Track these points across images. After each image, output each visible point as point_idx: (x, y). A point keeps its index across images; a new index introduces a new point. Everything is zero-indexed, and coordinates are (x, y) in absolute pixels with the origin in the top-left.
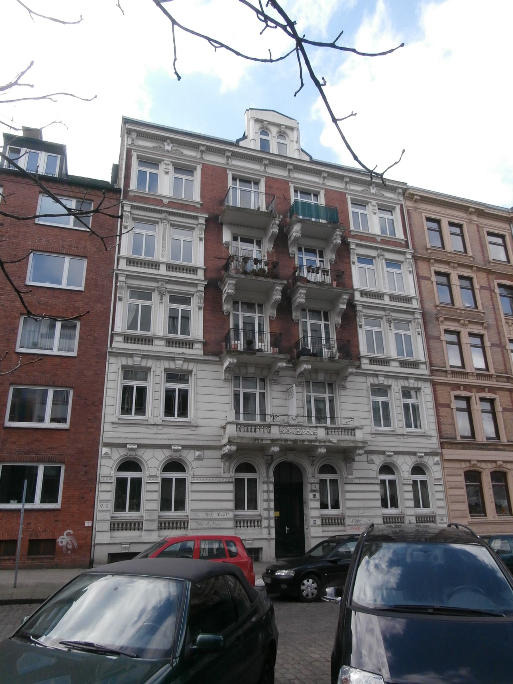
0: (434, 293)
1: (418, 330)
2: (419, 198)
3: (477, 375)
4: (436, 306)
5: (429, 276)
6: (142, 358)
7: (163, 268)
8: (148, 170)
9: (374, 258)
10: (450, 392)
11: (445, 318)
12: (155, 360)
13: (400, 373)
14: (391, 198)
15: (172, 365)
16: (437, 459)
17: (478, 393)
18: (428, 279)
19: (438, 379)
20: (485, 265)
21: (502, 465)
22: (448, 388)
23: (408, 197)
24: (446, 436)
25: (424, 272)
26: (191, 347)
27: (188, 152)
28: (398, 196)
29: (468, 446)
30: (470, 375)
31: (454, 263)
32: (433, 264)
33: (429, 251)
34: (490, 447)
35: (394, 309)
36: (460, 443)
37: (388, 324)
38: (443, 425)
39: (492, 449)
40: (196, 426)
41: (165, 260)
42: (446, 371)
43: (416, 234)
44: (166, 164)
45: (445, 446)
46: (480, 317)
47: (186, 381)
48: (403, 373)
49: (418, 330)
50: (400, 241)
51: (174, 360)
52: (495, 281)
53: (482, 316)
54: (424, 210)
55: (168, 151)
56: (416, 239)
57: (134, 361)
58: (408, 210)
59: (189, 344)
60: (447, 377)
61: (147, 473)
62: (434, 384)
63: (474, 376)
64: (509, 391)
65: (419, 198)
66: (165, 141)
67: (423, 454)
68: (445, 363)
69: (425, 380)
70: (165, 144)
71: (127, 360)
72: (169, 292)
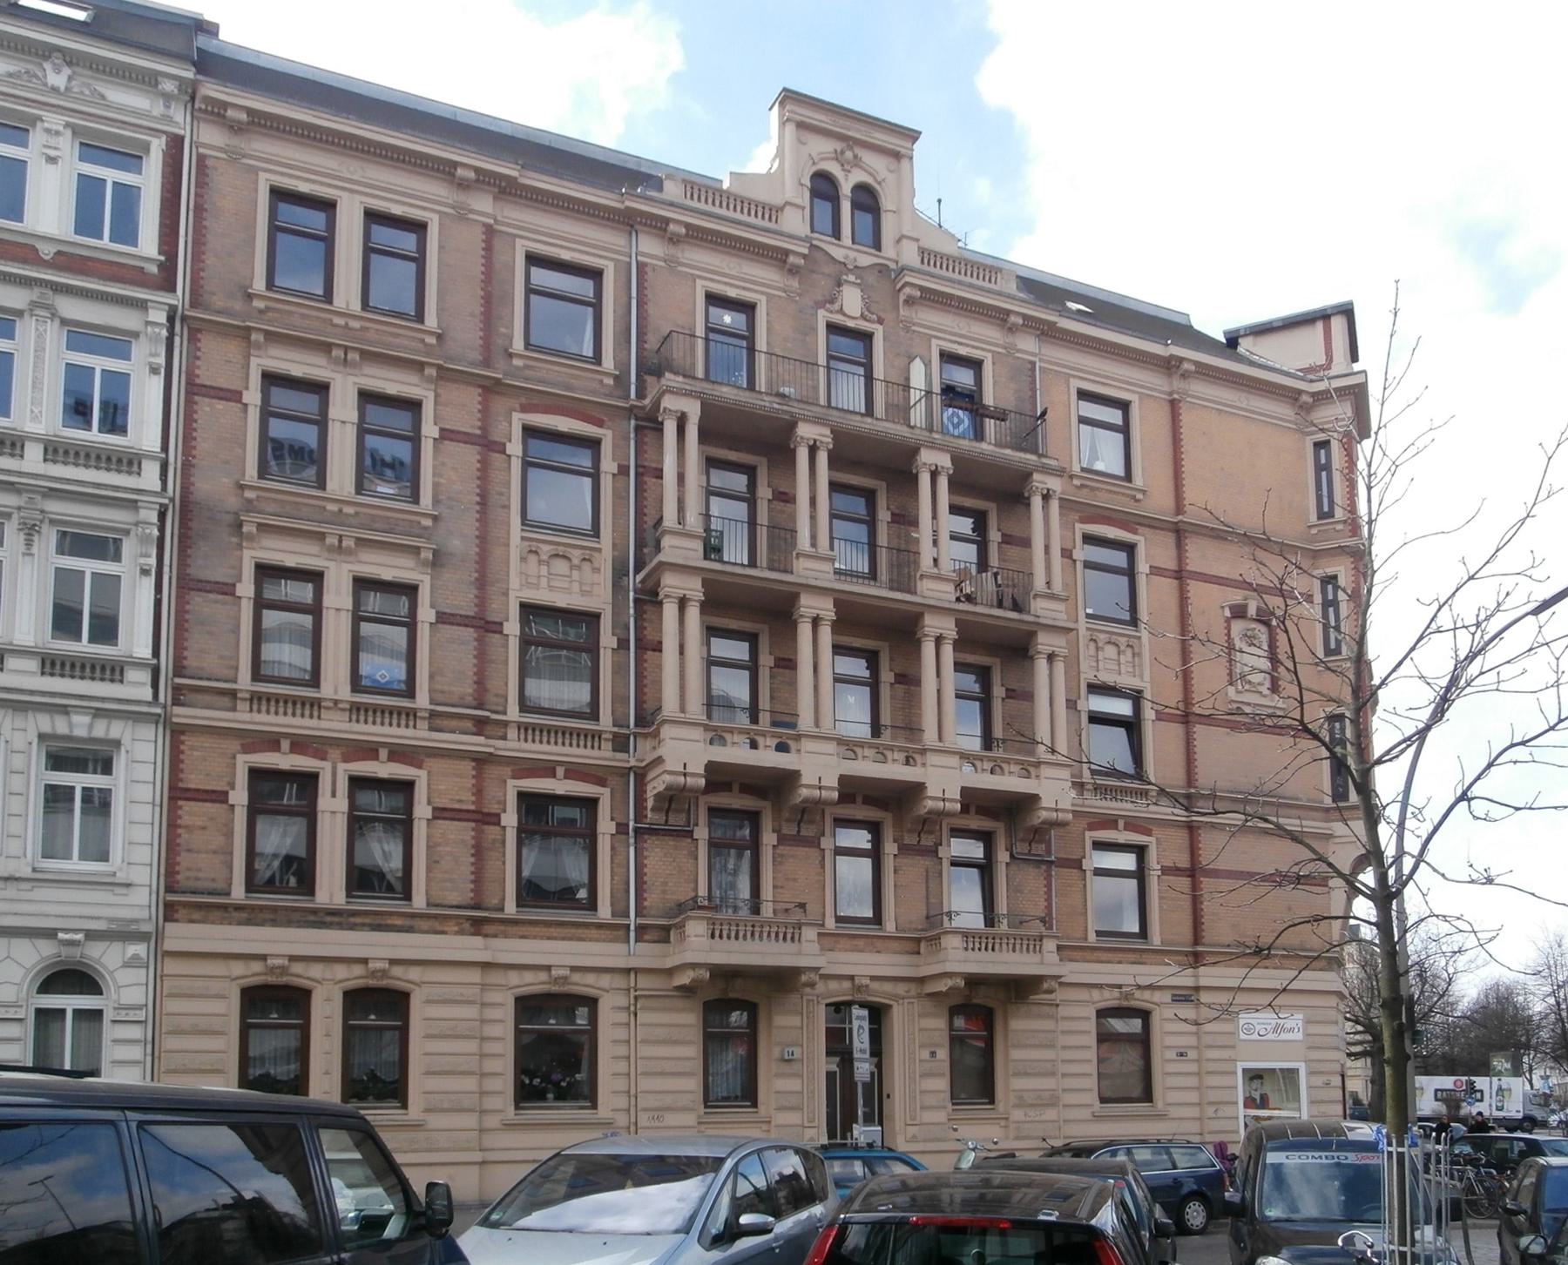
0: (243, 446)
1: (142, 561)
2: (243, 117)
3: (251, 700)
4: (242, 487)
5: (235, 385)
6: (95, 716)
7: (34, 453)
8: (111, 175)
9: (20, 313)
10: (234, 757)
11: (259, 525)
12: (10, 712)
13: (32, 692)
14: (135, 112)
15: (61, 726)
16: (139, 949)
17: (346, 760)
18: (234, 396)
19: (182, 715)
20: (487, 363)
21: (565, 978)
22: (235, 745)
23: (206, 111)
24: (192, 884)
25: (214, 372)
26: (117, 677)
27: (118, 95)
28: (168, 107)
29: (268, 916)
30: (327, 708)
31: (346, 349)
32: (258, 346)
33: (1076, 482)
34: (358, 920)
35: (51, 489)
36: (239, 908)
37: (22, 536)
38: (183, 854)
39: (364, 925)
40: (129, 885)
41: (39, 429)
42: (233, 694)
43: (213, 242)
44: (48, 131)
45: (182, 913)
46: (416, 531)
47: (106, 767)
48: (43, 693)
49: (142, 561)
50: (142, 264)
51: (67, 713)
52: (1078, 526)
53: (426, 528)
54: (520, 228)
55: (55, 90)
56: (210, 260)
57: (71, 725)
58: (201, 159)
59: (113, 671)
60: (234, 709)
61: (114, 996)
62: (177, 733)
63: (343, 710)
64: (474, 760)
65: (243, 117)
66: (46, 58)
67: (80, 936)
68: (237, 668)
69: (137, 718)
70: (47, 66)
71: (53, 722)
72: (52, 522)
